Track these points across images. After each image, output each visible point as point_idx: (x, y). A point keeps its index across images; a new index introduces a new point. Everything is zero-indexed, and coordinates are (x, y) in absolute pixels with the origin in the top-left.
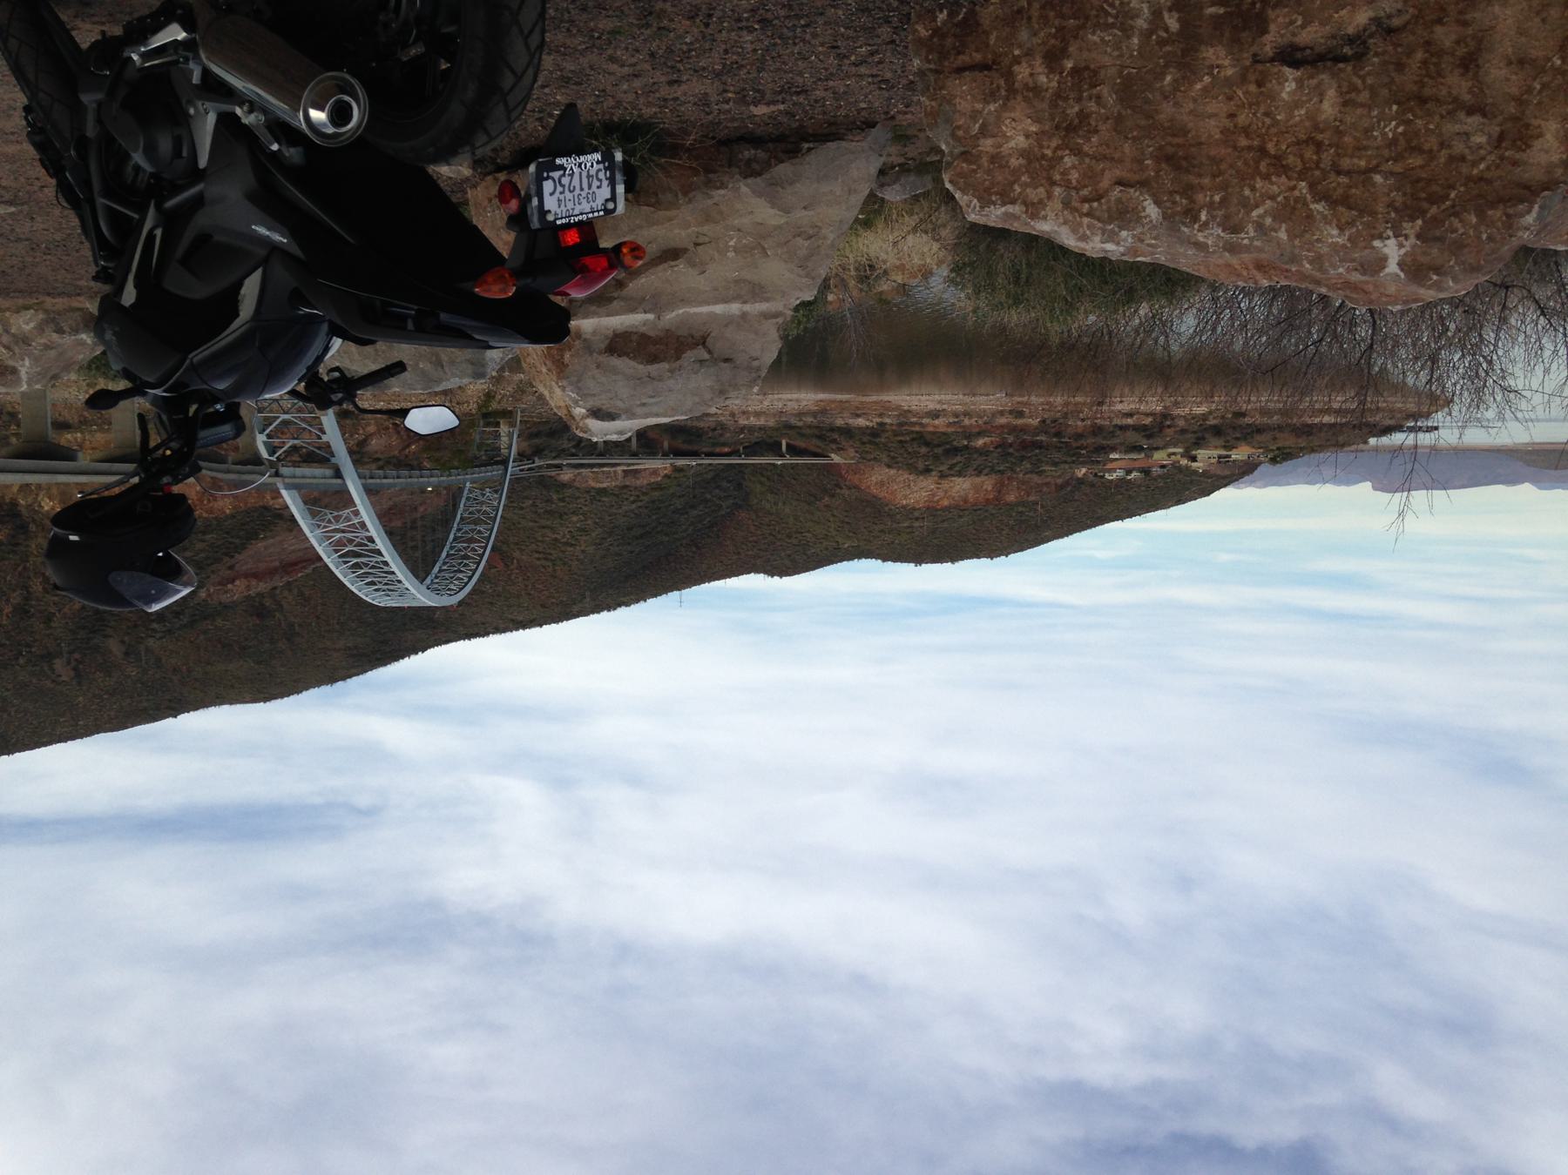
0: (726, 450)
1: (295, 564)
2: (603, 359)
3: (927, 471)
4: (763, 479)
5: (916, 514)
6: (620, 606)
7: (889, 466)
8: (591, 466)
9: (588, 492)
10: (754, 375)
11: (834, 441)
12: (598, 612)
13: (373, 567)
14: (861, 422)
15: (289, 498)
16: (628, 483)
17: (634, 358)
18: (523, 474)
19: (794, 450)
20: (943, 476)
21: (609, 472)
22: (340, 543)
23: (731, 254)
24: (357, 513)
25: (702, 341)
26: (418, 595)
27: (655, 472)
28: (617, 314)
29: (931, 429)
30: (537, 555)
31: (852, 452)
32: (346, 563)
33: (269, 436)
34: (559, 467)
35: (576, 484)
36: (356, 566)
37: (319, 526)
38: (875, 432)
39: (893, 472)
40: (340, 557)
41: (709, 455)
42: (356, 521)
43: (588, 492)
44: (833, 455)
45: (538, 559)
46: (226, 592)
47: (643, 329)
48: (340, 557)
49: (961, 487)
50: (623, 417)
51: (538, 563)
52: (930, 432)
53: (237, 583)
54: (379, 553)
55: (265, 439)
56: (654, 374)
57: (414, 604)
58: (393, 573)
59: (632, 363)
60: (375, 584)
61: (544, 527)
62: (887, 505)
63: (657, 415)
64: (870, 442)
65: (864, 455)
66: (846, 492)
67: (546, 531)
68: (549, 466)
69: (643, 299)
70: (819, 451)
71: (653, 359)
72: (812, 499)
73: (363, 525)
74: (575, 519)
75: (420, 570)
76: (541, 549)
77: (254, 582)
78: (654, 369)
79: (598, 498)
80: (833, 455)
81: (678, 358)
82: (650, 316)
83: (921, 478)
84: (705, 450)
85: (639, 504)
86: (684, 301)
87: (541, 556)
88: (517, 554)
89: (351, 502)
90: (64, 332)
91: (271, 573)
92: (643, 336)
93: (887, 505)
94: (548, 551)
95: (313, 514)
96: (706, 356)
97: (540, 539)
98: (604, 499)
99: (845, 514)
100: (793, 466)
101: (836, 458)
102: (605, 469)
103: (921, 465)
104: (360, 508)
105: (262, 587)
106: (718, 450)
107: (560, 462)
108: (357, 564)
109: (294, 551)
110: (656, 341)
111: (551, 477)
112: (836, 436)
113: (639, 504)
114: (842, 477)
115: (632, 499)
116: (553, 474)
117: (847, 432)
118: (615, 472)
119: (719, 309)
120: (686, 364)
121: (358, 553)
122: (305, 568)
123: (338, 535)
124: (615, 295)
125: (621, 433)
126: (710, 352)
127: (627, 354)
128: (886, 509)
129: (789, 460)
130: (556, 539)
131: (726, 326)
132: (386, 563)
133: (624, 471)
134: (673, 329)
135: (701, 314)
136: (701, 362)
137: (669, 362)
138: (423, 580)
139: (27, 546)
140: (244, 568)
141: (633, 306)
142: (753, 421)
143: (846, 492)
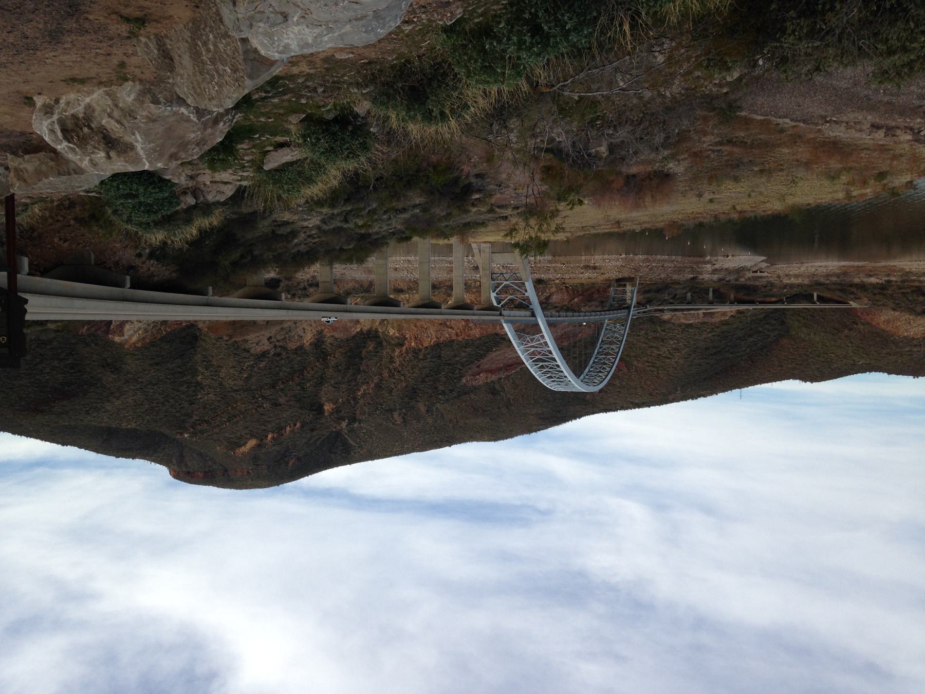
0: (774, 299)
1: (511, 365)
5: (915, 342)
6: (700, 397)
7: (894, 310)
9: (680, 326)
11: (853, 293)
12: (686, 400)
13: (551, 368)
14: (873, 280)
15: (508, 329)
16: (706, 321)
19: (821, 299)
22: (533, 353)
24: (543, 337)
26: (576, 385)
27: (724, 314)
30: (647, 364)
31: (865, 300)
32: (536, 365)
33: (497, 294)
34: (662, 311)
35: (673, 321)
36: (542, 367)
37: (522, 344)
38: (882, 288)
39: (897, 314)
41: (761, 303)
42: (542, 342)
43: (680, 326)
44: (851, 303)
45: (649, 366)
51: (648, 368)
53: (481, 375)
54: (554, 360)
57: (574, 390)
58: (562, 372)
61: (651, 347)
62: (892, 336)
64: (880, 294)
68: (656, 311)
70: (841, 299)
74: (671, 342)
75: (577, 371)
76: (650, 360)
77: (490, 375)
79: (687, 330)
83: (919, 317)
85: (714, 334)
87: (650, 364)
88: (635, 363)
89: (541, 332)
91: (499, 369)
93: (892, 336)
94: (654, 361)
95: (520, 337)
97: (649, 354)
98: (690, 330)
99: (859, 342)
100: (822, 310)
101: (853, 304)
102: (692, 312)
105: (494, 378)
106: (768, 299)
109: (510, 358)
112: (854, 290)
113: (714, 334)
114: (859, 317)
115: (709, 330)
117: (863, 287)
121: (543, 360)
122: (516, 368)
123: (533, 349)
129: (818, 306)
132: (558, 366)
140: (485, 367)
142: (793, 280)
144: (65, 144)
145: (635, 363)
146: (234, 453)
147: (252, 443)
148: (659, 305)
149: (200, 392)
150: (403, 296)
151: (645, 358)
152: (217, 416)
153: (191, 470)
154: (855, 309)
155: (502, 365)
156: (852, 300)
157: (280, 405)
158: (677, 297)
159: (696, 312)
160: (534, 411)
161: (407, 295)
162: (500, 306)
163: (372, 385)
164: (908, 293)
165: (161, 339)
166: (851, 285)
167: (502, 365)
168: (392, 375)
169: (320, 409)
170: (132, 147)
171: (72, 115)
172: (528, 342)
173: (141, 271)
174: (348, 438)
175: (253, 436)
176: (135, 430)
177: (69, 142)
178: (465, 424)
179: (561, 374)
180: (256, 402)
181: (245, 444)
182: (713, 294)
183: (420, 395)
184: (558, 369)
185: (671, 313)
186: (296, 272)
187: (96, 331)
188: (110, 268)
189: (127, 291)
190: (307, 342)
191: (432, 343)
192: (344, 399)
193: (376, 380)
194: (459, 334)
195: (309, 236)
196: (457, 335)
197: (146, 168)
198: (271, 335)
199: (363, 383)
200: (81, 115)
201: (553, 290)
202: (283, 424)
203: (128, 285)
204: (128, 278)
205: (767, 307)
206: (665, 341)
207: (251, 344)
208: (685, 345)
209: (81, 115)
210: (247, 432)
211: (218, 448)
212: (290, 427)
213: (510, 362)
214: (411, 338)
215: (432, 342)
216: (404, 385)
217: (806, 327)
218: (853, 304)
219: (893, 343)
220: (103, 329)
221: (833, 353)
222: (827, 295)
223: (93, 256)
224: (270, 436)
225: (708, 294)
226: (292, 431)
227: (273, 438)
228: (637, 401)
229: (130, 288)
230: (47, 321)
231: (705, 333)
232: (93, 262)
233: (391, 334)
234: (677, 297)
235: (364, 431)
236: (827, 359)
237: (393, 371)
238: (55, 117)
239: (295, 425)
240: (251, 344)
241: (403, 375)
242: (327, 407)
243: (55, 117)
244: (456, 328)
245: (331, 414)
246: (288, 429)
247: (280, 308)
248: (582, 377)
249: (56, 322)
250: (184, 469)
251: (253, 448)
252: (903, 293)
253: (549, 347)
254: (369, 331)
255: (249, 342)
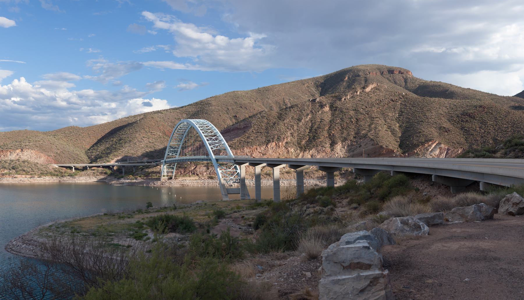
1: (226, 132)
2: (372, 263)
3: (24, 162)
4: (81, 159)
5: (27, 147)
8: (138, 163)
10: (327, 259)
17: (364, 263)
18: (158, 160)
19: (70, 168)
20: (18, 160)
21: (132, 161)
22: (216, 139)
23: (350, 292)
24: (212, 148)
25: (344, 268)
28: (370, 275)
29: (23, 176)
30: (155, 134)
31: (51, 168)
33: (236, 172)
34: (148, 162)
39: (36, 161)
40: (216, 135)
41: (99, 167)
42: (212, 146)
44: (57, 167)
46: (246, 124)
47: (362, 271)
48: (216, 135)
49: (12, 156)
50: (362, 247)
51: (154, 132)
52: (23, 175)
55: (237, 171)
56: (357, 259)
58: (201, 130)
59: (364, 262)
60: (206, 126)
61: (153, 143)
63: (352, 247)
65: (46, 167)
66: (52, 154)
67: (152, 142)
68: (151, 162)
69: (364, 279)
70: (61, 168)
71: (358, 263)
72: (63, 152)
73: (210, 145)
74: (143, 145)
76: (153, 136)
77: (238, 127)
78: (356, 261)
79: (135, 153)
80: (57, 167)
81: (351, 263)
82: (362, 274)
83: (26, 159)
84: (100, 168)
85: (122, 150)
86: (354, 278)
87: (153, 134)
88: (161, 134)
89: (212, 151)
90: (394, 234)
92: (361, 269)
94: (151, 135)
96: (342, 264)
97: (153, 139)
98: (133, 152)
99: (52, 147)
100: (70, 163)
101: (56, 166)
102: (133, 162)
103: (26, 163)
104: (211, 150)
106: (96, 168)
107: (148, 164)
108: (212, 133)
110: (357, 268)
111: (150, 159)
112: (56, 173)
115: (124, 152)
116: (150, 160)
118: (130, 161)
119: (344, 277)
120: (348, 262)
123: (216, 142)
124: (372, 280)
125: (359, 242)
126: (342, 265)
127: (366, 264)
128: (38, 149)
129: (72, 165)
130: (148, 139)
131: (340, 272)
132: (203, 133)
133: (127, 161)
134: (353, 271)
135: (348, 275)
136: (344, 262)
137: (354, 262)
138: (191, 127)
139: (297, 138)
140: (241, 131)
141: (366, 277)
143: (52, 154)
144: (420, 224)
145: (161, 134)
146: (377, 84)
147: (368, 89)
148: (149, 165)
149: (397, 117)
150: (287, 170)
151: (155, 137)
152: (387, 104)
153: (400, 75)
154: (55, 164)
155: (232, 132)
156: (56, 168)
157: (353, 110)
158: (141, 169)
159: (131, 162)
160: (213, 108)
161: (284, 170)
162: (235, 165)
163: (303, 121)
164: (32, 171)
165: (418, 146)
166: (57, 175)
167: (232, 132)
168: (292, 126)
169: (331, 107)
170: (401, 223)
171: (418, 231)
172: (220, 146)
173: (427, 184)
174: (315, 92)
175: (368, 93)
176: (431, 97)
177: (419, 225)
178: (250, 100)
179: (202, 129)
180: (367, 111)
181: (372, 89)
182: (122, 171)
183: (276, 116)
184: (203, 131)
185: (143, 161)
186: (346, 183)
187: (454, 151)
188: (443, 185)
189: (433, 173)
190: (339, 144)
191: (270, 144)
192: (318, 113)
193: (301, 124)
194: (255, 149)
195: (340, 202)
196: (257, 149)
197: (398, 218)
198: (360, 148)
199: (308, 122)
200: (415, 231)
201: (205, 174)
202: (351, 99)
203: (433, 176)
204: (433, 180)
205: (96, 164)
206: (146, 146)
207: (370, 143)
208: (136, 144)
209: (415, 231)
210: (371, 95)
211: (386, 87)
212: (347, 98)
213: (227, 134)
214: (282, 147)
215: (270, 145)
216: (285, 121)
217: (78, 154)
218: (56, 166)
219: (37, 146)
220: (450, 151)
221: (64, 141)
222: (69, 171)
223: (451, 191)
224: (358, 93)
225: (125, 171)
226: (347, 96)
227: (357, 92)
228: (160, 114)
229: (432, 175)
230: (474, 157)
231: (126, 151)
232: (451, 188)
233: (293, 149)
234: (141, 169)
235: (306, 95)
236: (67, 138)
237: (291, 128)
238: (423, 231)
239: (345, 99)
240: (370, 143)
241: (286, 127)
242: (327, 109)
243: (423, 231)
244: (257, 152)
245: (325, 105)
246: (349, 97)
247: (355, 164)
248: (190, 127)
249: (469, 157)
250: (404, 75)
251: (367, 86)
252: (34, 171)
253: (209, 143)
254: (305, 151)
255: (371, 144)
